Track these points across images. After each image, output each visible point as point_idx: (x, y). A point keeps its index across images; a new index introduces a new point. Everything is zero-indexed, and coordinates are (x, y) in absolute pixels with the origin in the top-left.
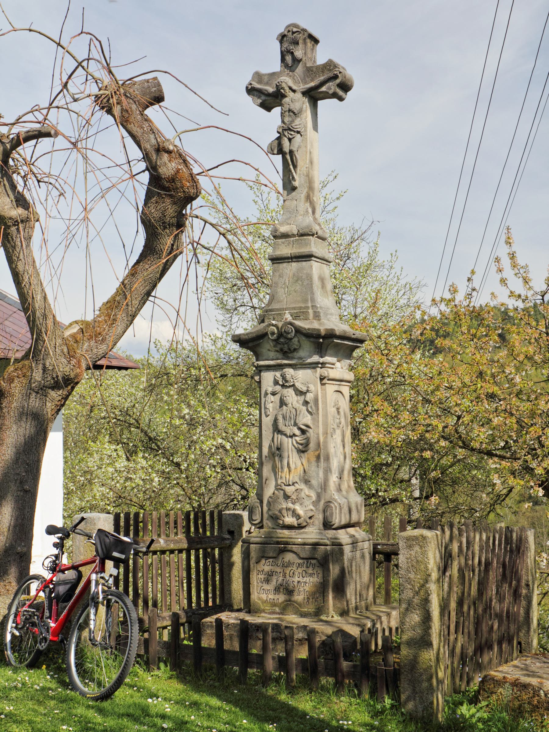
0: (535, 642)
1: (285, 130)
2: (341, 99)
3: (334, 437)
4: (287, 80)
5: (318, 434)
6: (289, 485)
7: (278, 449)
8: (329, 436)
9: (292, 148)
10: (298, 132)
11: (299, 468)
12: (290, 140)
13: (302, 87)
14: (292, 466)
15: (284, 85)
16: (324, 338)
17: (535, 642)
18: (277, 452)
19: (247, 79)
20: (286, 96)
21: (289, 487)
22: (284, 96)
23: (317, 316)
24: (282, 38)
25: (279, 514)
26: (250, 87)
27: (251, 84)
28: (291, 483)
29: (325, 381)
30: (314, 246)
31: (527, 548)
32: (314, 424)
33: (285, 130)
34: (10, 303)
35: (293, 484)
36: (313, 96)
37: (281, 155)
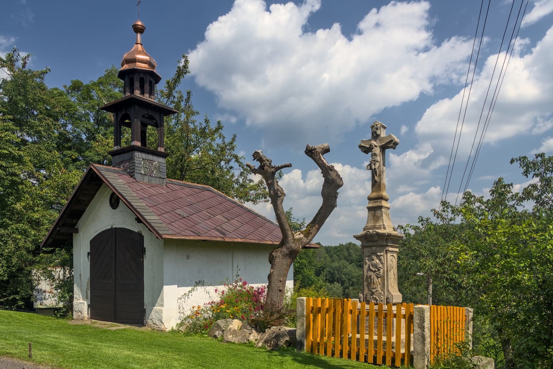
2: (394, 149)
12: (374, 164)
14: (375, 282)
19: (359, 143)
22: (373, 148)
23: (385, 228)
24: (253, 155)
30: (384, 203)
31: (446, 71)
34: (276, 225)
36: (383, 148)
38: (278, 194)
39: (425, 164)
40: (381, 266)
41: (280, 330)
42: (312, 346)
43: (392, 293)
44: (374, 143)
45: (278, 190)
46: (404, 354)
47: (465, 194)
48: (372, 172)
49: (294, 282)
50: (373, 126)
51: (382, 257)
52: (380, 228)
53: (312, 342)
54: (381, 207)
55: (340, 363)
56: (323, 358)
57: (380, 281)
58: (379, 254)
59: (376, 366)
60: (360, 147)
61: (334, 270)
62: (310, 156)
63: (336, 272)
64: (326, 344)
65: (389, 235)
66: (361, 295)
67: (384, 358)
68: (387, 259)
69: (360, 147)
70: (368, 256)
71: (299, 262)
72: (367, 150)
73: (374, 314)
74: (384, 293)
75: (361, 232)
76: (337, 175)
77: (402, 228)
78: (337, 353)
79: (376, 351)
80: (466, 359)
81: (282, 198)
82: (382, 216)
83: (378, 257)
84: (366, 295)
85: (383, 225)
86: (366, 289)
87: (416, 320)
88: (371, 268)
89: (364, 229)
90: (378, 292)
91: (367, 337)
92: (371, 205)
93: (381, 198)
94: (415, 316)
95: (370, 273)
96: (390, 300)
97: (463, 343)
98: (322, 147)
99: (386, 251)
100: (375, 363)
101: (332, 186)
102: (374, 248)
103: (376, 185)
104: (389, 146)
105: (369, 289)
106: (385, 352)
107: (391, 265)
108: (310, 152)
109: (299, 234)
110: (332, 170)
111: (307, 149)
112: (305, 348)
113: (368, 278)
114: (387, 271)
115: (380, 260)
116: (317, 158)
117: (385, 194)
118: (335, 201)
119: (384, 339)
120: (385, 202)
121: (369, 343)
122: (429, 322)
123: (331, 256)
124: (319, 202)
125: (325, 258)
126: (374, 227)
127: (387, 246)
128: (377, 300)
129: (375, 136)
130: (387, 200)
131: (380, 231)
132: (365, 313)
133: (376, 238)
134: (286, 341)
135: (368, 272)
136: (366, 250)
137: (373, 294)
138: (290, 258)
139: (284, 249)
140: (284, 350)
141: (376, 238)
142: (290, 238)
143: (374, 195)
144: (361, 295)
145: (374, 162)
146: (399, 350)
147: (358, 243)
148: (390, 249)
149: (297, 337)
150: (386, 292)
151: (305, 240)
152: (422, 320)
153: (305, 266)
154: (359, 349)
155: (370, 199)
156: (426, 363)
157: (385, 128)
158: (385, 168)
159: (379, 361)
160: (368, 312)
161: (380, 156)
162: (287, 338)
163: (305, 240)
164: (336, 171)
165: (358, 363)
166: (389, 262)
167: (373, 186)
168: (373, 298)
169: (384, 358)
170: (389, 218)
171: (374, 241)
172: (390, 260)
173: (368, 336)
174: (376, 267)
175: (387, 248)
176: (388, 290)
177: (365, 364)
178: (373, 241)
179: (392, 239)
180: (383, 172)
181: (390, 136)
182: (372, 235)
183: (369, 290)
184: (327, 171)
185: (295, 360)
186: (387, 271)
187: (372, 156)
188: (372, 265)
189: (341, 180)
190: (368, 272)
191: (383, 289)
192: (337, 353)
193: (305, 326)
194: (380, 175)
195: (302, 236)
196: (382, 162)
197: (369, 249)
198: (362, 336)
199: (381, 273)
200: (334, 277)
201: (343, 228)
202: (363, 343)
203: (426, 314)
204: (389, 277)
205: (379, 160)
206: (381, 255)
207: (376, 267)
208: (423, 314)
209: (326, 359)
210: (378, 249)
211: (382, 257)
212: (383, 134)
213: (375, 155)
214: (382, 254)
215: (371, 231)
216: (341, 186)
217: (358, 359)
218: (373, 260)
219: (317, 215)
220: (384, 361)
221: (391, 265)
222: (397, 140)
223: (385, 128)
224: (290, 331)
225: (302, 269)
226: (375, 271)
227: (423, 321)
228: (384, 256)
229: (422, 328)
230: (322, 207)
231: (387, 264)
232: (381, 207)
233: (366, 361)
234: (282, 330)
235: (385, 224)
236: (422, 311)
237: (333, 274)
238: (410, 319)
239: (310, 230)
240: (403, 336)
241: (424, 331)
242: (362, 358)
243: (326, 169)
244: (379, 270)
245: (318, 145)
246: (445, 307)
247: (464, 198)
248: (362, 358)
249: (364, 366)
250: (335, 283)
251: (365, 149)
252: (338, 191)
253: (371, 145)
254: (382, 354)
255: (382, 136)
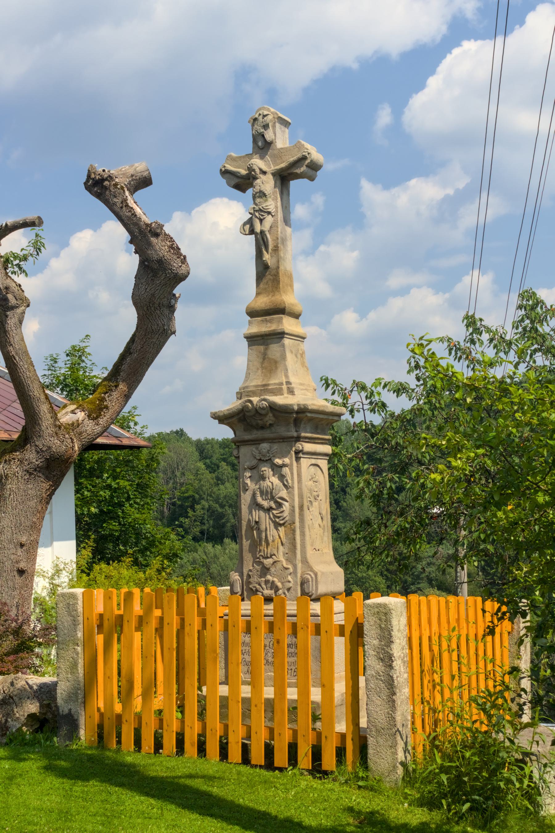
0: (477, 798)
1: (257, 211)
2: (312, 179)
3: (311, 509)
4: (258, 163)
5: (293, 507)
6: (267, 558)
7: (257, 523)
8: (305, 508)
9: (263, 228)
10: (269, 213)
11: (276, 541)
12: (261, 221)
13: (273, 168)
14: (270, 539)
15: (255, 167)
16: (298, 412)
17: (477, 798)
18: (471, 352)
20: (257, 178)
21: (268, 560)
22: (255, 178)
23: (291, 391)
25: (258, 586)
26: (223, 169)
27: (224, 167)
28: (269, 555)
29: (301, 455)
30: (288, 324)
32: (290, 498)
33: (257, 211)
35: (271, 557)
36: (284, 178)
37: (254, 236)
38: (6, 300)
39: (449, 208)
40: (284, 493)
41: (12, 684)
42: (101, 727)
43: (316, 568)
44: (258, 163)
45: (7, 288)
46: (343, 736)
47: (522, 296)
48: (257, 240)
49: (78, 545)
50: (255, 120)
51: (286, 470)
52: (278, 391)
53: (102, 715)
54: (280, 335)
55: (173, 769)
56: (129, 759)
57: (282, 534)
58: (278, 461)
59: (271, 773)
60: (225, 173)
61: (222, 506)
62: (99, 196)
63: (229, 511)
64: (139, 717)
65: (303, 411)
66: (235, 576)
67: (293, 748)
68: (299, 475)
69: (225, 173)
70: (252, 468)
71: (109, 487)
72: (242, 182)
73: (263, 629)
74: (295, 566)
75: (229, 403)
76: (171, 247)
77: (363, 388)
78: (169, 742)
79: (271, 731)
80: (501, 736)
81: (19, 310)
82: (284, 357)
83: (277, 469)
84: (249, 576)
85: (288, 383)
86: (248, 558)
87: (371, 639)
88: (259, 499)
89: (240, 395)
90: (279, 566)
91: (246, 691)
92: (255, 330)
93: (280, 311)
94: (366, 627)
95: (257, 515)
96: (311, 588)
97: (490, 695)
98: (131, 171)
99: (297, 453)
100: (269, 765)
101: (158, 281)
102: (265, 446)
103: (268, 277)
104: (298, 171)
105: (255, 557)
106: (295, 732)
107: (311, 491)
108: (99, 186)
109: (73, 412)
110: (157, 235)
111: (89, 176)
112: (82, 732)
113: (252, 529)
114: (301, 507)
115: (282, 478)
116: (118, 201)
117: (290, 299)
118: (170, 318)
119: (292, 694)
120: (292, 320)
121: (253, 709)
122: (404, 642)
123: (213, 468)
124: (127, 320)
125: (197, 474)
126: (265, 389)
127: (298, 439)
128: (277, 589)
129: (262, 145)
130: (296, 316)
131: (279, 400)
132: (241, 624)
133: (270, 419)
134: (31, 716)
135: (251, 513)
136: (245, 451)
137: (265, 570)
138: (48, 478)
139: (31, 455)
140: (24, 743)
141: (270, 419)
142: (46, 421)
143: (263, 302)
144: (235, 576)
145: (259, 213)
146: (331, 725)
147: (225, 433)
148: (308, 447)
149: (59, 701)
150: (299, 565)
151: (90, 427)
152: (387, 638)
153: (128, 499)
154: (226, 727)
155: (253, 313)
156: (401, 756)
157: (286, 124)
158: (289, 230)
159: (281, 758)
160: (248, 623)
161: (275, 199)
162: (33, 707)
163: (90, 427)
164: (168, 238)
165: (224, 766)
166: (307, 483)
167: (260, 278)
168: (267, 582)
169: (293, 748)
170: (303, 364)
171: (263, 427)
172: (306, 477)
173: (295, 690)
174: (272, 498)
175: (299, 446)
176: (305, 561)
177: (245, 769)
178: (263, 428)
179: (311, 420)
180: (284, 241)
181: (299, 146)
182: (258, 412)
183: (257, 561)
184: (143, 236)
185: (48, 768)
186: (301, 507)
187: (254, 197)
188: (262, 493)
189: (184, 260)
190: (251, 513)
191: (291, 559)
192: (169, 742)
193: (81, 670)
194: (276, 249)
195: (81, 415)
196: (280, 215)
197: (253, 448)
198: (234, 690)
199: (286, 514)
200: (224, 525)
201: (188, 395)
202: (236, 711)
203: (394, 622)
204: (308, 522)
205: (272, 208)
206: (284, 465)
207: (272, 498)
208: (388, 621)
209: (137, 762)
210: (275, 447)
211: (286, 470)
212: (281, 139)
213: (262, 195)
214: (287, 460)
215: (255, 400)
216: (182, 278)
217: (224, 754)
218: (263, 478)
219: (123, 357)
220: (293, 759)
221: (311, 491)
222: (316, 155)
223: (286, 124)
224: (42, 686)
225: (120, 505)
226: (270, 509)
227: (389, 642)
228: (290, 466)
229: (387, 660)
230: (134, 336)
231: (300, 489)
232: (280, 335)
233: (246, 760)
234: (21, 684)
235: (292, 379)
236: (384, 614)
237: (221, 516)
238: (357, 634)
239: (102, 400)
240: (340, 688)
241: (391, 667)
242: (235, 753)
243: (141, 231)
244: (280, 505)
245: (121, 170)
246: (423, 598)
247: (520, 307)
248: (235, 753)
249: (239, 773)
250: (227, 540)
251: (236, 181)
252: (177, 291)
253: (250, 169)
254: (287, 737)
255: (279, 144)
